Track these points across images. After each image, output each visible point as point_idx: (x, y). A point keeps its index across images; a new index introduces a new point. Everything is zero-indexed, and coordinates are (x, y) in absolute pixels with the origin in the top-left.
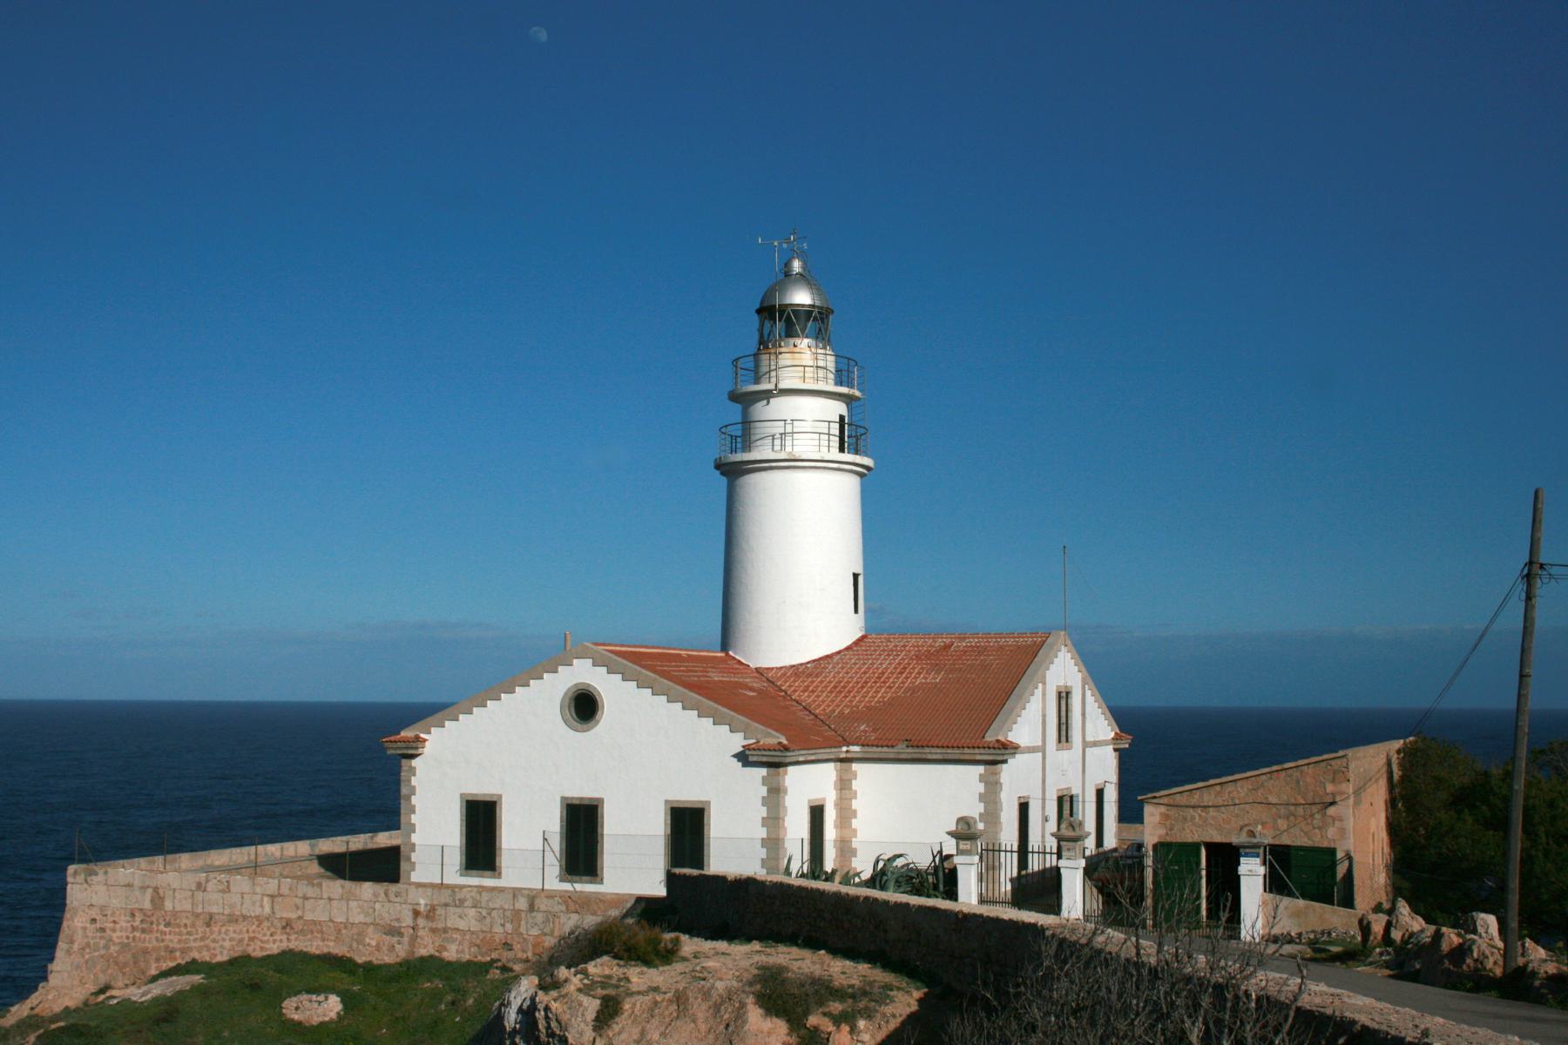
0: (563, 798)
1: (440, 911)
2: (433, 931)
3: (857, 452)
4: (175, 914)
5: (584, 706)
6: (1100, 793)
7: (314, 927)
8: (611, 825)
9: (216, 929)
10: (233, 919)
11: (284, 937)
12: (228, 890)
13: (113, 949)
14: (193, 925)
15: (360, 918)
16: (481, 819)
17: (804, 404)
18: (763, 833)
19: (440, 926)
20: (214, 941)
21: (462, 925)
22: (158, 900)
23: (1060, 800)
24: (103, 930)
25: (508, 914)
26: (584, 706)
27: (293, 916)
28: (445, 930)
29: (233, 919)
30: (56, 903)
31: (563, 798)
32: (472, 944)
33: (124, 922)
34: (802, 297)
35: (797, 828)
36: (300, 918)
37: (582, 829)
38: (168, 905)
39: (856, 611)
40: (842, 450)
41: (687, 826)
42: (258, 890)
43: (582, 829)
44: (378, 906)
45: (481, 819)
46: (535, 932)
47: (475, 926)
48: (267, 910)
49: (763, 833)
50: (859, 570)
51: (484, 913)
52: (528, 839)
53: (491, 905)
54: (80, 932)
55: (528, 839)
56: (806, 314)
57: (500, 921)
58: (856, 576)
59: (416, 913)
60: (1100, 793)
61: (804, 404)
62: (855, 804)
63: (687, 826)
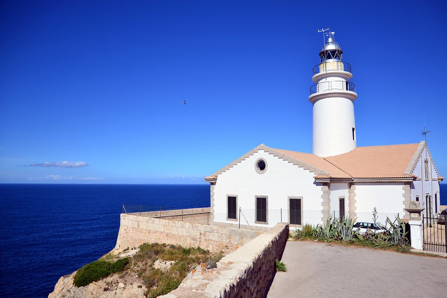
0: (256, 196)
1: (207, 233)
2: (206, 240)
3: (352, 90)
4: (142, 229)
5: (262, 165)
6: (436, 195)
7: (173, 236)
8: (240, 204)
9: (151, 234)
10: (156, 232)
11: (166, 239)
12: (153, 223)
13: (129, 238)
14: (146, 233)
15: (186, 234)
16: (232, 202)
17: (332, 76)
18: (322, 208)
19: (207, 238)
20: (150, 238)
21: (214, 239)
22: (138, 225)
23: (427, 197)
24: (127, 232)
25: (227, 236)
26: (262, 165)
27: (169, 232)
28: (209, 240)
29: (156, 232)
30: (117, 226)
31: (256, 196)
32: (217, 246)
33: (131, 230)
34: (331, 47)
35: (336, 207)
36: (170, 233)
37: (261, 204)
38: (141, 227)
39: (354, 139)
40: (347, 90)
41: (295, 206)
42: (161, 223)
43: (261, 204)
44: (190, 230)
45: (232, 202)
46: (236, 243)
47: (218, 240)
48: (163, 230)
49: (322, 208)
50: (354, 127)
51: (220, 235)
52: (247, 208)
53: (222, 233)
54: (123, 232)
55: (247, 208)
56: (333, 52)
57: (225, 238)
58: (353, 129)
59: (201, 234)
60: (436, 195)
61: (332, 76)
62: (356, 198)
63: (295, 206)
